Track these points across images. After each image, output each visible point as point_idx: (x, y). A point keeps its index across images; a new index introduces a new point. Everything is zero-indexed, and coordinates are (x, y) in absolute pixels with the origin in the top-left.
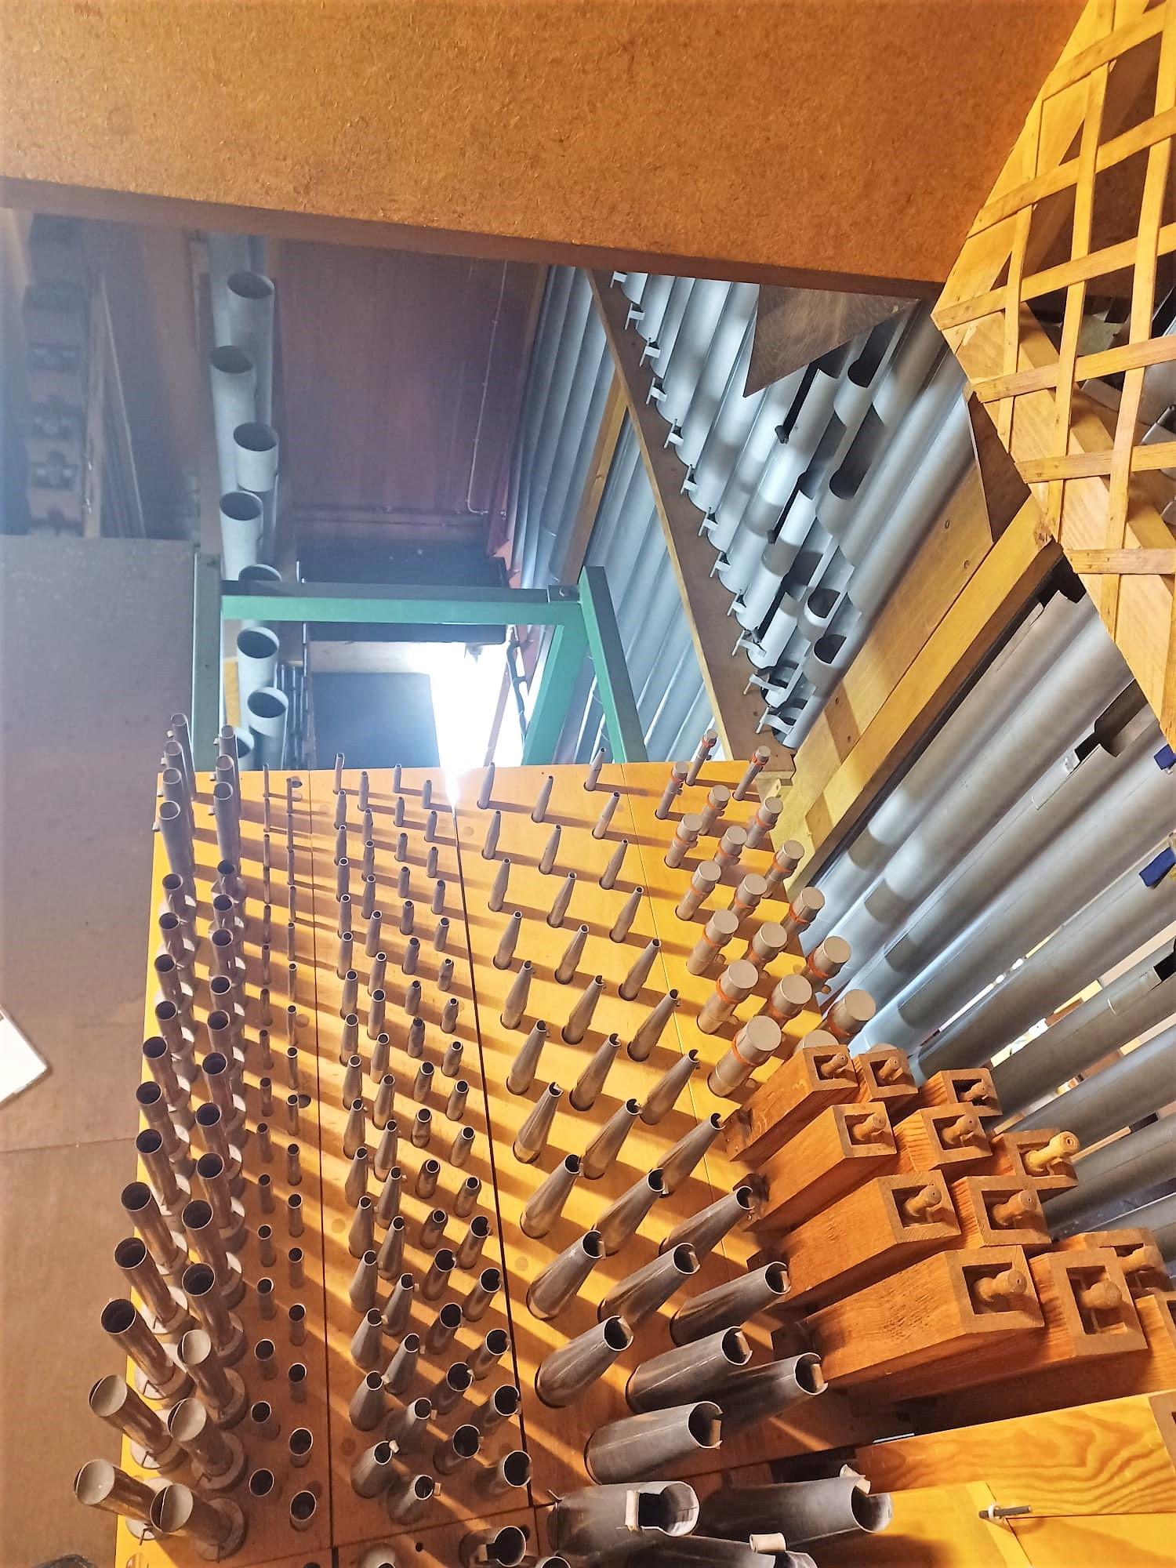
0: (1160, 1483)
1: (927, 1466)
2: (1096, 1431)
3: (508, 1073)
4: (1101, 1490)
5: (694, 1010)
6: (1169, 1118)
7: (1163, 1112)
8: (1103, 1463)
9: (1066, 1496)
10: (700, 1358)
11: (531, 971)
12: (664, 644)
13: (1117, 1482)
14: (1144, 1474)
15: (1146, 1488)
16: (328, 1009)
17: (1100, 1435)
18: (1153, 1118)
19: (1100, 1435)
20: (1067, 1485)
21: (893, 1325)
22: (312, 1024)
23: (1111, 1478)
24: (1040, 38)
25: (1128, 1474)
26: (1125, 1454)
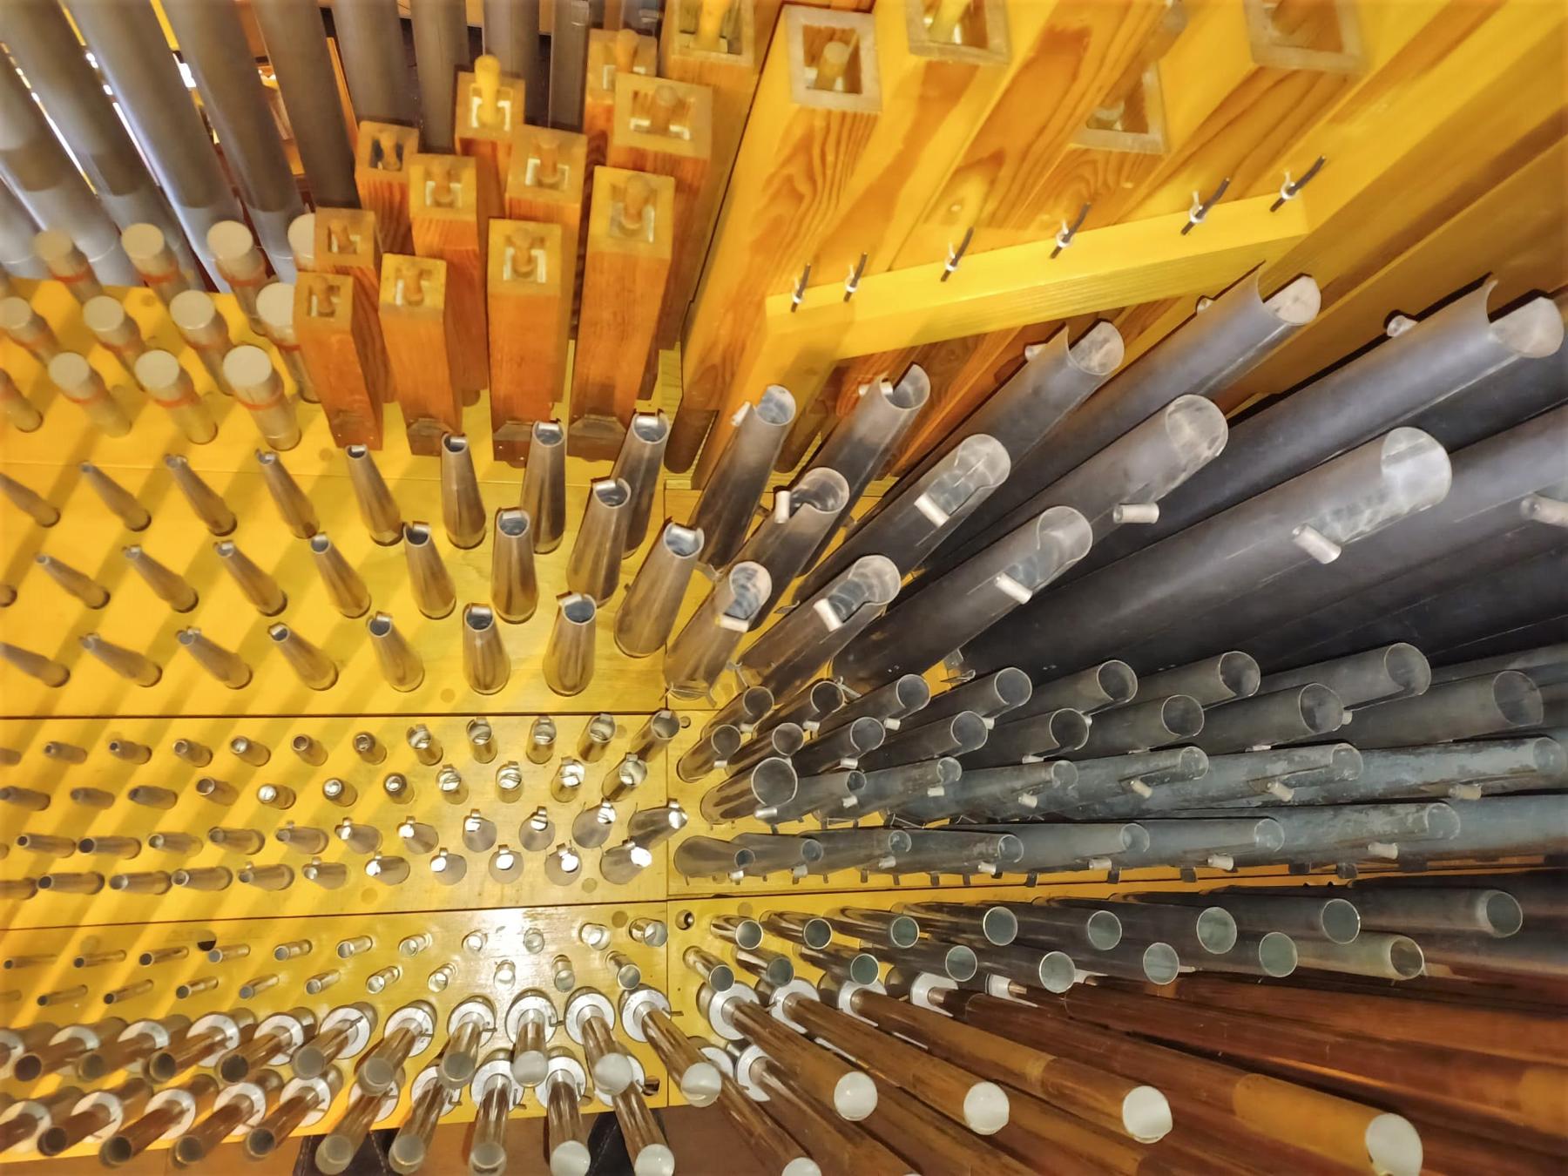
0: (851, 131)
1: (730, 345)
2: (785, 172)
3: (220, 685)
4: (827, 190)
5: (89, 440)
6: (413, 7)
7: (404, 13)
8: (812, 179)
9: (813, 227)
10: (604, 533)
11: (85, 639)
12: (1184, 814)
13: (829, 172)
14: (838, 143)
15: (847, 146)
16: (82, 910)
17: (792, 170)
18: (406, 25)
19: (792, 170)
20: (808, 219)
21: (623, 331)
22: (97, 931)
23: (824, 174)
24: (559, 1064)
25: (830, 158)
26: (816, 152)
